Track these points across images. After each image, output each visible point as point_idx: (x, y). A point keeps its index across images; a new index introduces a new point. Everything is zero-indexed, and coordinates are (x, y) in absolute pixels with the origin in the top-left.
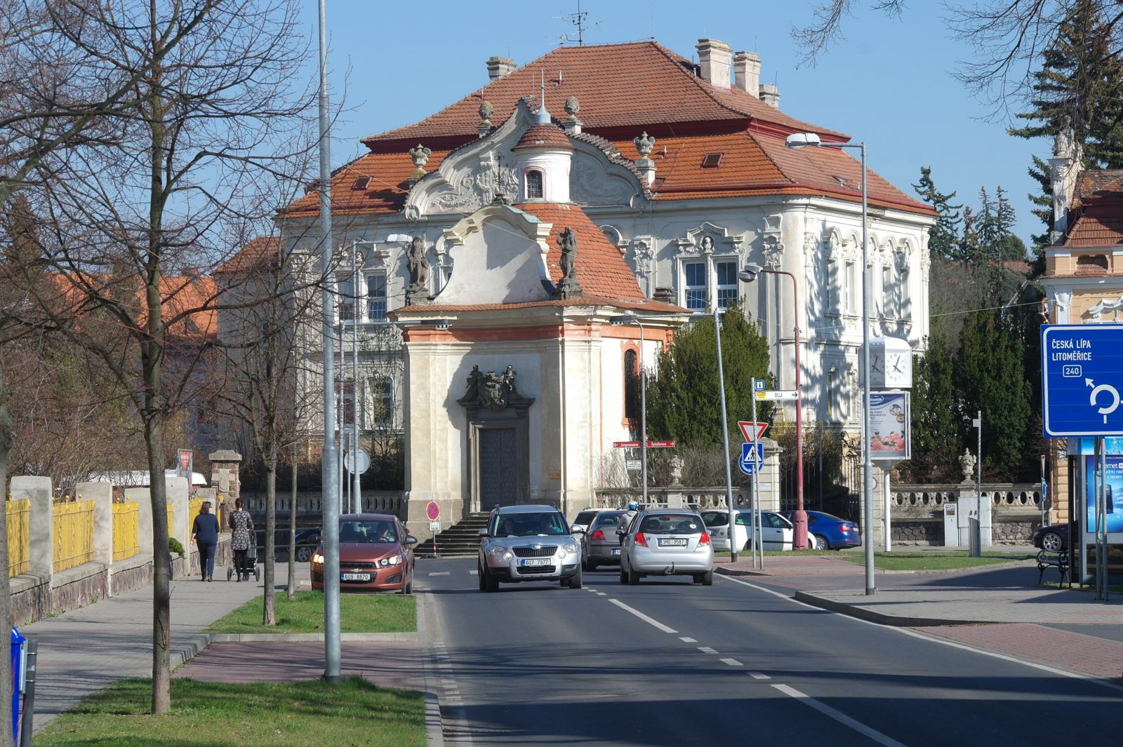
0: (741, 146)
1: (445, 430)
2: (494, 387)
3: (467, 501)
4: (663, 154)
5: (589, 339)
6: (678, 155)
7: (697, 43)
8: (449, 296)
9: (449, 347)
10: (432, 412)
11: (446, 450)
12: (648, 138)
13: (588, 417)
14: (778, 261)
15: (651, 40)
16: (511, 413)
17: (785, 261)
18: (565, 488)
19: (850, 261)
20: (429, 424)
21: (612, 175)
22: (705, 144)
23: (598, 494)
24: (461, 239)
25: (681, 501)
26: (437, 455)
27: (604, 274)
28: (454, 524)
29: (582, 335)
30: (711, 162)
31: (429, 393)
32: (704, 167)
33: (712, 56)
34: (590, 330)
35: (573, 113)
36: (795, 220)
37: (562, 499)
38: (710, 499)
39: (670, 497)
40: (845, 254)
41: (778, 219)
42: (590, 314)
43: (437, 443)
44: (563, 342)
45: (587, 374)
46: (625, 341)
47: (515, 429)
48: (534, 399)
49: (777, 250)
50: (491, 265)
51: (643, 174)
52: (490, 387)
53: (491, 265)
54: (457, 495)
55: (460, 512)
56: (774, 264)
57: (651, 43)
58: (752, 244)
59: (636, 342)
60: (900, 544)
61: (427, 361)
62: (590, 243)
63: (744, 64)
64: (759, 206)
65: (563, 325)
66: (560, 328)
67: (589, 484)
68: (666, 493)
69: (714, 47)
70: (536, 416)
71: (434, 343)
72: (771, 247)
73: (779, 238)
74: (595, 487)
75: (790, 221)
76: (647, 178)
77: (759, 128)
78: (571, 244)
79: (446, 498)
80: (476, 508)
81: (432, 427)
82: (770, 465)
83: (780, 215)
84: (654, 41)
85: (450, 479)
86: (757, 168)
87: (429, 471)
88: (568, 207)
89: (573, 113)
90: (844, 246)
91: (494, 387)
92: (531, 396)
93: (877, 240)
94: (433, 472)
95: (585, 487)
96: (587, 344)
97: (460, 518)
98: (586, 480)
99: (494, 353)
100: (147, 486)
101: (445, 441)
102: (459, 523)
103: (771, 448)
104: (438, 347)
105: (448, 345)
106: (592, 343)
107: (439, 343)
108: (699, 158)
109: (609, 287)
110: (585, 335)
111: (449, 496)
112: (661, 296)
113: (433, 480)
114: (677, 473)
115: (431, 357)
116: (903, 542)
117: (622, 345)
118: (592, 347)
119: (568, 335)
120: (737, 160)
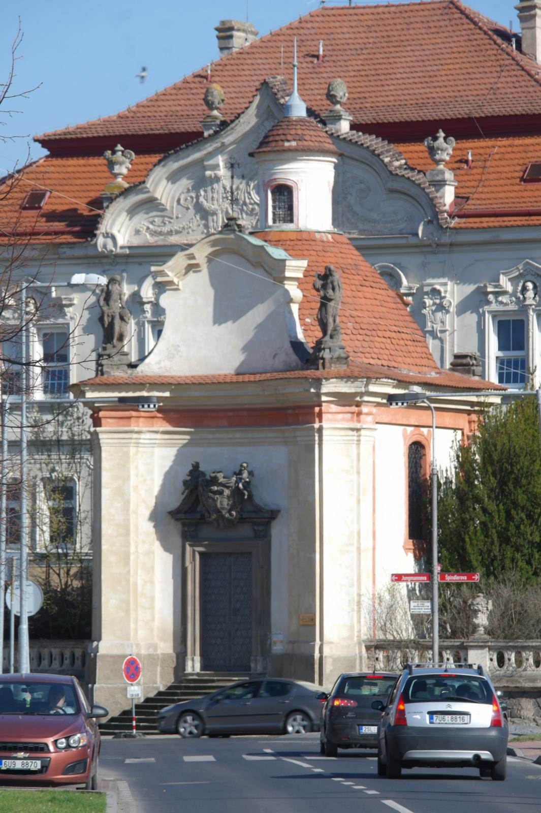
1: (150, 553)
2: (221, 493)
4: (467, 162)
8: (159, 363)
9: (159, 436)
11: (152, 583)
12: (445, 139)
16: (246, 530)
18: (321, 639)
20: (127, 545)
21: (392, 191)
24: (176, 280)
26: (139, 590)
27: (380, 333)
28: (162, 689)
29: (347, 421)
32: (525, 181)
34: (359, 414)
35: (338, 102)
37: (317, 655)
42: (359, 390)
43: (139, 572)
44: (320, 430)
46: (410, 429)
47: (250, 553)
48: (278, 511)
61: (126, 455)
66: (317, 409)
67: (356, 634)
68: (465, 648)
70: (280, 534)
71: (136, 429)
74: (364, 637)
76: (442, 197)
78: (333, 289)
79: (151, 651)
80: (194, 665)
81: (132, 549)
85: (157, 624)
88: (330, 236)
89: (338, 102)
91: (221, 493)
92: (274, 507)
94: (132, 616)
95: (351, 637)
96: (355, 433)
97: (170, 680)
101: (150, 570)
102: (170, 688)
104: (143, 436)
106: (363, 432)
107: (144, 429)
108: (518, 168)
109: (387, 352)
110: (352, 420)
111: (156, 649)
113: (132, 626)
114: (482, 620)
115: (132, 450)
118: (362, 438)
119: (328, 420)
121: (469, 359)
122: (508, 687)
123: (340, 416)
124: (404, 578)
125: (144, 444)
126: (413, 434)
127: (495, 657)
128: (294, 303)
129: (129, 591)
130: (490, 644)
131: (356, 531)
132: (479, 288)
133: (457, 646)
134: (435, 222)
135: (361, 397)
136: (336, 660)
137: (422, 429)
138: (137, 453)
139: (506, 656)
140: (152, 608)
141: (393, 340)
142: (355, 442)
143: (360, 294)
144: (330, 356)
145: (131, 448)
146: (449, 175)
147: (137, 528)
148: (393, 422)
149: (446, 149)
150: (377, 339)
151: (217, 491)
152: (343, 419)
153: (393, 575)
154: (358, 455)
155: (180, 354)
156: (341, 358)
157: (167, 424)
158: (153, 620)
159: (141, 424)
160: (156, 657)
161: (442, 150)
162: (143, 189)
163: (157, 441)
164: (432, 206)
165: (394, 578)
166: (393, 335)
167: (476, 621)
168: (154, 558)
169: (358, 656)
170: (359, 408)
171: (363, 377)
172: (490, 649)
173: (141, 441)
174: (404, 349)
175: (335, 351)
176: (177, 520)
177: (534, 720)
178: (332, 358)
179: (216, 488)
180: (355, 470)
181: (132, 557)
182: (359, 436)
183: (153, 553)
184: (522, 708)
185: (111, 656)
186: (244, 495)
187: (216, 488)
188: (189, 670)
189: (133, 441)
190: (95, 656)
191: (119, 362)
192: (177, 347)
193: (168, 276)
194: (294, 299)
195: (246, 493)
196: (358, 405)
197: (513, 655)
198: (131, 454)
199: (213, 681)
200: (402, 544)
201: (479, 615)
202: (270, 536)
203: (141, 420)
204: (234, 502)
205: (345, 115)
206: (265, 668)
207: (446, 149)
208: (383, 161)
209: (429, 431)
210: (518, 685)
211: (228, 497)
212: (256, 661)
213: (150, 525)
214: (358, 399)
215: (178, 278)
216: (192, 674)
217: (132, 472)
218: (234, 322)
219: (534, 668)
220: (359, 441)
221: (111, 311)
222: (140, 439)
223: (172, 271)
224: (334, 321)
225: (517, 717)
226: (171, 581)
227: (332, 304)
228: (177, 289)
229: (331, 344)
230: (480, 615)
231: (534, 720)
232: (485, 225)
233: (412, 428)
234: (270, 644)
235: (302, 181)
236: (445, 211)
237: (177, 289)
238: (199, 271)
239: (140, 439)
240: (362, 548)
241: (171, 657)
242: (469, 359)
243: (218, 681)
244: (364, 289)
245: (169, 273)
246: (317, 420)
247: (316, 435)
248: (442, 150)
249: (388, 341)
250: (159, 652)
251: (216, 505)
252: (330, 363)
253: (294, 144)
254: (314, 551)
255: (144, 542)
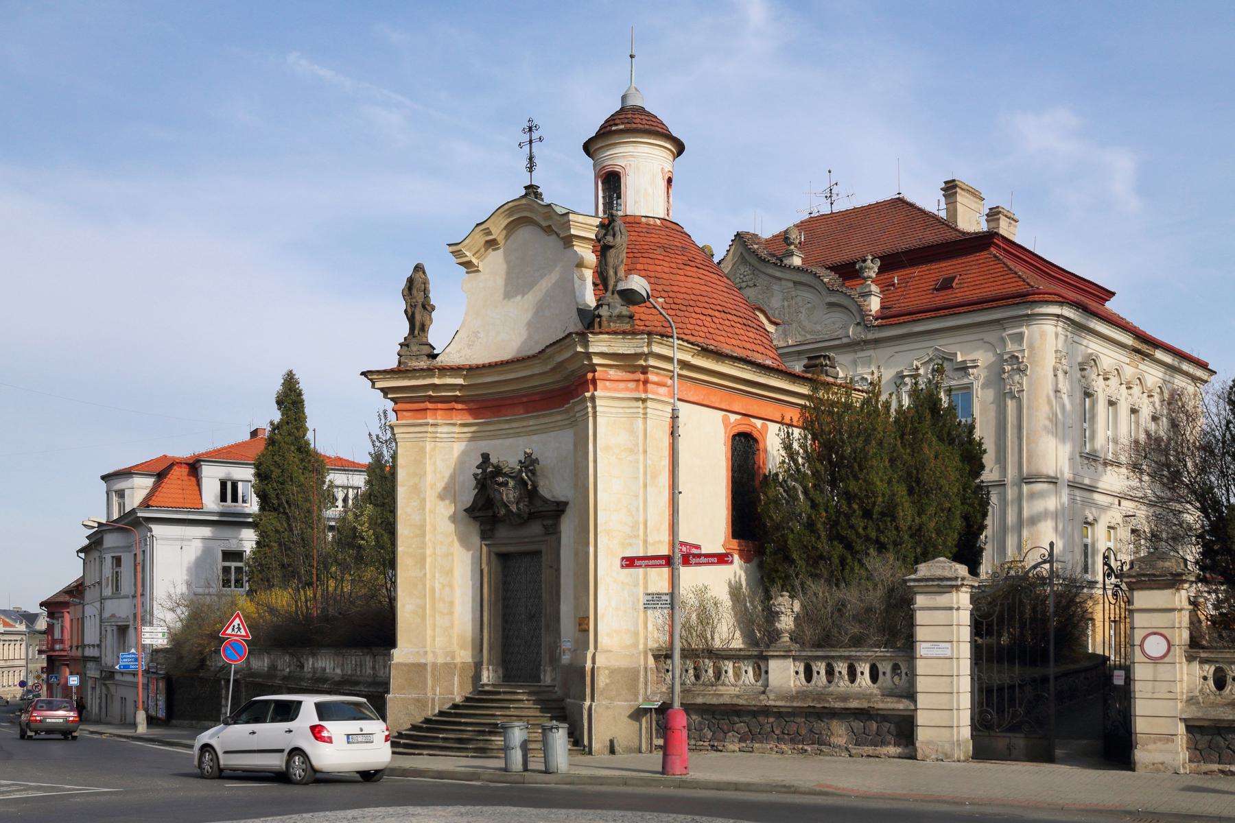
0: (981, 266)
1: (449, 555)
2: (506, 484)
3: (478, 666)
4: (893, 285)
5: (643, 396)
6: (909, 284)
7: (943, 185)
8: (459, 352)
9: (457, 429)
10: (428, 528)
11: (451, 587)
12: (872, 260)
13: (642, 527)
14: (1021, 384)
15: (898, 196)
16: (536, 529)
17: (1030, 384)
18: (596, 648)
19: (1114, 399)
20: (423, 546)
21: (831, 305)
22: (941, 270)
23: (657, 657)
24: (475, 261)
25: (793, 674)
26: (437, 594)
27: (697, 310)
28: (458, 699)
29: (631, 390)
30: (947, 285)
31: (424, 500)
32: (937, 290)
33: (959, 198)
34: (646, 382)
35: (792, 243)
36: (1043, 334)
37: (589, 665)
38: (841, 667)
39: (773, 665)
40: (1107, 389)
41: (1021, 335)
42: (639, 350)
43: (437, 575)
44: (593, 398)
45: (641, 458)
46: (733, 418)
47: (538, 553)
48: (566, 504)
49: (1021, 371)
50: (508, 295)
51: (865, 301)
52: (501, 484)
53: (508, 295)
54: (465, 656)
55: (470, 680)
56: (1016, 389)
57: (898, 198)
58: (988, 367)
59: (759, 423)
60: (1222, 772)
61: (423, 450)
62: (682, 266)
63: (999, 219)
64: (997, 321)
65: (595, 371)
66: (590, 376)
67: (642, 641)
68: (766, 659)
69: (963, 189)
70: (567, 526)
71: (431, 421)
72: (1013, 369)
73: (1023, 357)
74: (652, 644)
75: (1037, 336)
76: (869, 305)
77: (1004, 249)
78: (614, 236)
79: (448, 660)
80: (487, 676)
81: (428, 552)
82: (951, 609)
83: (1024, 329)
84: (901, 196)
85: (456, 631)
86: (999, 283)
87: (424, 618)
88: (658, 222)
89: (792, 243)
90: (1106, 379)
91: (506, 484)
92: (563, 499)
93: (1145, 381)
94: (429, 622)
95: (636, 645)
96: (640, 404)
97: (468, 691)
98: (636, 634)
99: (517, 435)
100: (922, 658)
101: (449, 573)
102: (467, 699)
103: (954, 575)
104: (440, 429)
105: (454, 425)
106: (649, 404)
107: (440, 421)
108: (934, 283)
109: (705, 330)
110: (637, 389)
111: (453, 658)
112: (815, 366)
113: (429, 632)
114: (786, 623)
115: (429, 446)
116: (1227, 767)
117: (725, 421)
118: (649, 411)
119: (606, 389)
120: (976, 279)
121: (822, 359)
122: (814, 707)
123: (622, 385)
124: (637, 563)
125: (442, 438)
126: (738, 423)
127: (801, 669)
128: (586, 267)
129: (425, 595)
130: (794, 653)
131: (641, 519)
132: (897, 373)
133: (756, 656)
134: (862, 324)
135: (646, 360)
136: (613, 672)
137: (753, 420)
138: (434, 449)
139: (815, 669)
140: (451, 613)
141: (714, 319)
142: (641, 416)
143: (681, 272)
144: (609, 314)
145: (428, 443)
146: (874, 288)
147: (435, 529)
148: (704, 403)
149: (873, 268)
150: (694, 315)
151: (502, 482)
152: (627, 389)
153: (623, 559)
154: (645, 430)
155: (480, 340)
156: (623, 316)
157: (470, 418)
158: (452, 626)
159: (439, 417)
160: (453, 666)
161: (869, 268)
162: (510, 215)
163: (456, 436)
164: (862, 312)
165: (624, 563)
166: (717, 314)
167: (778, 626)
168: (453, 560)
169: (642, 667)
170: (646, 376)
171: (642, 333)
172: (794, 659)
173: (438, 435)
174: (731, 329)
175: (615, 307)
176: (475, 518)
177: (847, 749)
178: (610, 316)
179: (501, 479)
180: (641, 449)
181: (428, 560)
182: (645, 408)
183: (452, 554)
184: (832, 734)
185: (405, 665)
186: (527, 484)
187: (501, 479)
188: (485, 680)
189: (429, 435)
190: (1129, 679)
191: (418, 353)
192: (476, 333)
193: (466, 256)
194: (586, 262)
195: (530, 483)
196: (644, 370)
197: (731, 665)
198: (428, 449)
199: (499, 693)
200: (305, 403)
201: (782, 618)
202: (560, 532)
203: (440, 412)
204: (520, 494)
205: (796, 252)
206: (554, 680)
207: (873, 268)
208: (822, 280)
209: (763, 425)
210: (827, 705)
211: (514, 488)
212: (545, 671)
213: (452, 527)
214: (642, 362)
215: (478, 258)
216: (487, 685)
217: (429, 469)
218: (523, 296)
219: (848, 683)
220: (645, 414)
221: (414, 300)
222: (437, 432)
223: (469, 250)
224: (616, 273)
225: (826, 745)
226: (470, 583)
227: (612, 251)
228: (478, 271)
229: (610, 300)
230: (783, 618)
231: (847, 749)
232: (901, 321)
233: (739, 417)
234: (560, 653)
235: (630, 165)
236: (870, 315)
237: (478, 271)
238: (498, 249)
239: (437, 432)
240: (650, 540)
241: (470, 666)
242: (822, 359)
243: (505, 693)
244: (688, 268)
245: (467, 254)
246: (591, 387)
247: (589, 404)
248: (869, 268)
249: (709, 319)
250: (458, 660)
251: (502, 499)
252: (609, 322)
253: (622, 127)
254: (588, 544)
255: (442, 543)
